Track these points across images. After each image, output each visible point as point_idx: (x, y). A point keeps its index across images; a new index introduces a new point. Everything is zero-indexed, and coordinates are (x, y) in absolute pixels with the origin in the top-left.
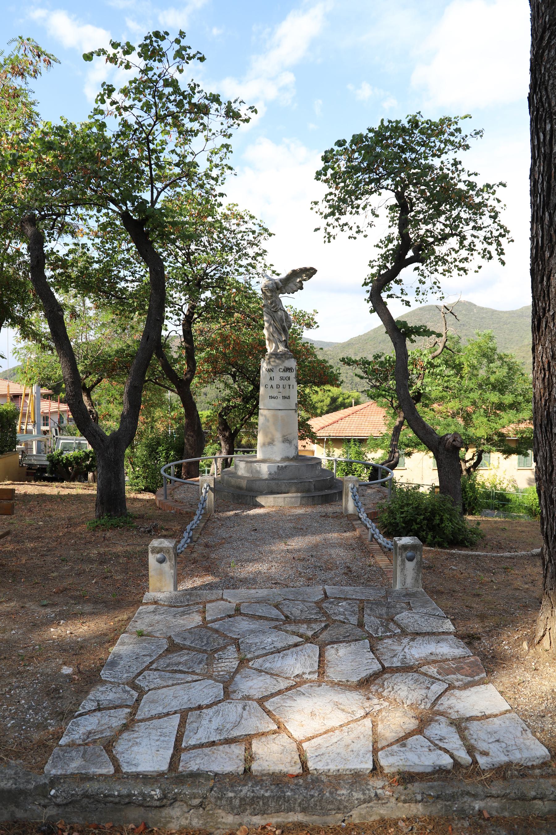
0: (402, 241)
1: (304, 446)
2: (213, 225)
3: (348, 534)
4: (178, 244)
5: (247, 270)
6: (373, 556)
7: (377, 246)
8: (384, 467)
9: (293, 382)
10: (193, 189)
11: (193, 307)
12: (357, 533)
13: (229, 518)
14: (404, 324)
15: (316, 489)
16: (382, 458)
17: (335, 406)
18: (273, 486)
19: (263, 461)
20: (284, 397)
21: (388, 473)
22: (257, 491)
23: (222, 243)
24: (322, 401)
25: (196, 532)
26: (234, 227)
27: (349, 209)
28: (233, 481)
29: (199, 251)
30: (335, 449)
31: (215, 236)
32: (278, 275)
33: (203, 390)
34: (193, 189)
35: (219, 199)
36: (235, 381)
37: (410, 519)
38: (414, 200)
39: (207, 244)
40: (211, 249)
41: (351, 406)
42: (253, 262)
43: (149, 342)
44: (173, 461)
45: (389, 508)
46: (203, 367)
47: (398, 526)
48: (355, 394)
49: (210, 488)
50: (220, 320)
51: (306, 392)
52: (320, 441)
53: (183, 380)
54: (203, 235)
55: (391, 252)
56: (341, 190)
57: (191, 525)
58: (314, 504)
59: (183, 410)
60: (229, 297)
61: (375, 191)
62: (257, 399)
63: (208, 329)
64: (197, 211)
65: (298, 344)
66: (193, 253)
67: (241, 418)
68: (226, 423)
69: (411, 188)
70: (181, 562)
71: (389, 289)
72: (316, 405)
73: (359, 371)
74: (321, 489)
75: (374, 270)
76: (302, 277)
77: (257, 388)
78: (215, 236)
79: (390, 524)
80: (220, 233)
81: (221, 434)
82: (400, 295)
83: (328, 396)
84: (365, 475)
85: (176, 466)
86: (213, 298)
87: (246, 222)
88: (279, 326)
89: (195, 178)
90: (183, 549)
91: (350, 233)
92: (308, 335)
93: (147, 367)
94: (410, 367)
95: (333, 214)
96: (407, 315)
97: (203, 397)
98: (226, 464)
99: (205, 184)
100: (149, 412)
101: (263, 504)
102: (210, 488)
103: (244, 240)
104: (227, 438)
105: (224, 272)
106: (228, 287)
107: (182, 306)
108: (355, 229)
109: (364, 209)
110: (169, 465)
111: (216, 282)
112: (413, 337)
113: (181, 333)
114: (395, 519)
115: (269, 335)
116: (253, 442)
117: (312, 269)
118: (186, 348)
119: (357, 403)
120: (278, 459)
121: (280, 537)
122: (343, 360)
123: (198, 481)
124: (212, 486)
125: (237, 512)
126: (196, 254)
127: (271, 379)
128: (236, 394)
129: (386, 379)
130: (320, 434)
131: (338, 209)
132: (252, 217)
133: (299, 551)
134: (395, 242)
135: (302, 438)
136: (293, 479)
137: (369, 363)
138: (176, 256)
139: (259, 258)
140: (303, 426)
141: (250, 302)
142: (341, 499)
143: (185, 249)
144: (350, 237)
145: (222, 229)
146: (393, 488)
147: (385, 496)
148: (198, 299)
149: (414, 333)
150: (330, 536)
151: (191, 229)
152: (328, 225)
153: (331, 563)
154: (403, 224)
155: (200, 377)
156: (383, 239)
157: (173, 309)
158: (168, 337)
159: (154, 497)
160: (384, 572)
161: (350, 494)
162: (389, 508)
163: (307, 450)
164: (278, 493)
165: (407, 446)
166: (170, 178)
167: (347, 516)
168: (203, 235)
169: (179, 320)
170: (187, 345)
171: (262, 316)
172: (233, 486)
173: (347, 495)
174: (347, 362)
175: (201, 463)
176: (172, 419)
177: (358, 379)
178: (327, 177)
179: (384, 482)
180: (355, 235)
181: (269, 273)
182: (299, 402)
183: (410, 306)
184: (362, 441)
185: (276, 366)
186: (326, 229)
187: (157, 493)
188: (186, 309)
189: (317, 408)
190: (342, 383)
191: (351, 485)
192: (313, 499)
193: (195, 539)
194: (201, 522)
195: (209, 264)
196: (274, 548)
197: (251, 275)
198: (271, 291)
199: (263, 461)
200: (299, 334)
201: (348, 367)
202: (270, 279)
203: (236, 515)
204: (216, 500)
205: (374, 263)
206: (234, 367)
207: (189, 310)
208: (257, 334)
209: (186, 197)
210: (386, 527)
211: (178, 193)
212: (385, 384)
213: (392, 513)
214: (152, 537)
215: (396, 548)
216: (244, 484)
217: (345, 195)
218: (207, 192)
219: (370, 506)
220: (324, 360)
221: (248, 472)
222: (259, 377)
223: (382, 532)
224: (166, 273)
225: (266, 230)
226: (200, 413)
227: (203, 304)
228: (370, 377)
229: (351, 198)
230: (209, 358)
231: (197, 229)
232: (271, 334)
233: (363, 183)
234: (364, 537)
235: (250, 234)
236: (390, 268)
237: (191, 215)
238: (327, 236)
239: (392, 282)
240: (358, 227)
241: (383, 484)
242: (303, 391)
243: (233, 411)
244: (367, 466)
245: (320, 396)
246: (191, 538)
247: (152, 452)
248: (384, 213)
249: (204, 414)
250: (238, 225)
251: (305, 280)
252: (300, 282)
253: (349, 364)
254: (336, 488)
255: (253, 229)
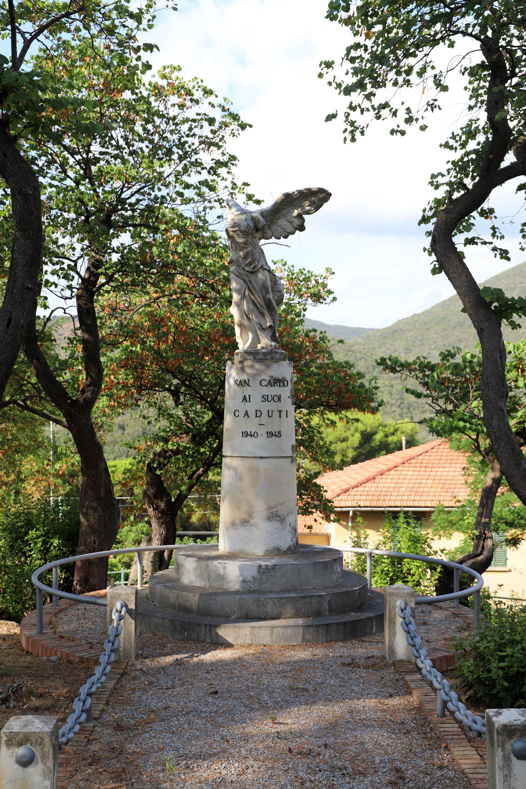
0: (493, 133)
1: (310, 527)
2: (134, 108)
3: (396, 702)
4: (67, 141)
5: (199, 195)
6: (446, 748)
7: (447, 145)
8: (464, 566)
9: (287, 404)
10: (92, 37)
11: (96, 264)
12: (414, 699)
13: (164, 669)
14: (498, 294)
15: (334, 610)
16: (461, 550)
17: (369, 448)
18: (249, 610)
19: (231, 556)
20: (270, 434)
21: (472, 578)
22: (219, 616)
23: (151, 141)
24: (345, 440)
25: (98, 699)
26: (173, 112)
27: (392, 75)
28: (172, 596)
29: (107, 157)
30: (369, 532)
31: (138, 128)
32: (258, 202)
33: (117, 420)
34: (92, 37)
35: (145, 56)
36: (177, 403)
37: (518, 672)
38: (519, 53)
39: (122, 142)
40: (131, 154)
41: (400, 449)
42: (210, 178)
43: (11, 330)
44: (57, 557)
45: (476, 648)
46: (115, 376)
47: (495, 686)
48: (407, 426)
49: (129, 611)
50: (150, 289)
51: (313, 423)
52: (342, 516)
53: (77, 401)
54: (115, 125)
55: (473, 156)
56: (377, 38)
57: (88, 685)
58: (329, 641)
59: (78, 458)
60: (165, 244)
61: (443, 39)
62: (220, 437)
63: (123, 305)
64: (102, 80)
65: (297, 332)
66: (97, 160)
67: (190, 472)
68: (162, 483)
69: (513, 30)
70: (67, 762)
71: (469, 227)
72: (332, 448)
73: (413, 383)
74: (344, 610)
75: (441, 193)
76: (302, 207)
77: (219, 416)
78: (138, 128)
79: (479, 681)
80: (147, 121)
81: (151, 503)
82: (489, 239)
83: (356, 430)
84: (428, 584)
85: (63, 567)
86: (135, 246)
87: (197, 102)
88: (259, 300)
89: (98, 14)
90: (71, 735)
91: (392, 123)
92: (315, 314)
93: (7, 378)
94: (511, 375)
95: (360, 85)
96: (506, 275)
97: (117, 434)
98: (161, 562)
99: (116, 27)
100: (13, 463)
101: (230, 640)
102: (129, 611)
103: (194, 135)
104: (163, 512)
105: (156, 197)
106: (163, 227)
107: (75, 262)
108: (402, 115)
109: (420, 74)
110: (49, 565)
111: (141, 216)
112: (515, 317)
113: (74, 312)
114: (489, 671)
115: (242, 317)
116: (213, 519)
117: (321, 191)
118: (84, 342)
119: (411, 443)
120: (260, 551)
121: (264, 708)
122: (382, 362)
123: (105, 596)
124: (132, 606)
125: (179, 657)
126: (102, 163)
127: (245, 399)
128: (181, 428)
129: (465, 398)
130: (341, 503)
131: (371, 77)
132: (208, 92)
133: (301, 735)
134: (481, 138)
135: (306, 511)
136: (289, 591)
137: (432, 368)
138: (63, 165)
139: (222, 171)
140: (308, 487)
141: (204, 255)
142: (382, 630)
143: (79, 153)
144: (393, 132)
145: (152, 114)
146: (484, 609)
147: (468, 626)
148: (105, 249)
149: (516, 310)
150: (360, 704)
151: (92, 115)
152: (352, 108)
153: (363, 761)
154: (495, 104)
155: (110, 397)
156: (458, 132)
157: (57, 267)
158: (49, 319)
159: (17, 630)
160: (469, 781)
161: (399, 621)
162: (476, 648)
163: (316, 534)
164: (260, 619)
165: (511, 525)
166: (48, 13)
167: (394, 664)
168: (115, 125)
169: (70, 287)
170: (86, 336)
171: (227, 281)
172: (172, 606)
173: (393, 622)
174: (390, 365)
175: (112, 560)
176: (57, 475)
177: (412, 398)
178: (351, 13)
179: (466, 597)
180: (403, 126)
181: (240, 199)
182: (300, 443)
183: (508, 259)
184: (421, 517)
185: (254, 376)
186: (347, 115)
187: (24, 621)
188: (83, 266)
189: (333, 454)
190: (380, 405)
191: (399, 603)
192: (327, 631)
193: (96, 714)
194: (109, 679)
195: (128, 182)
196: (250, 729)
197: (206, 204)
198: (245, 233)
199: (231, 556)
200: (298, 315)
201: (391, 374)
202: (243, 212)
203: (178, 663)
204: (139, 635)
205: (440, 180)
206: (175, 377)
207: (88, 269)
208: (220, 315)
209: (81, 51)
210: (471, 687)
211: (64, 42)
212: (463, 406)
213: (483, 659)
214: (10, 712)
215: (491, 732)
216: (193, 600)
217: (383, 49)
218: (120, 44)
219: (439, 644)
220: (347, 363)
221: (200, 576)
222: (223, 395)
223: (464, 698)
224: (43, 197)
225: (235, 117)
226: (109, 463)
227: (115, 257)
228: (435, 394)
229: (396, 54)
230: (127, 359)
231: (102, 115)
232: (245, 315)
233: (419, 24)
234: (428, 706)
235: (206, 124)
236: (470, 187)
237: (91, 87)
238: (350, 129)
239: (475, 214)
240: (408, 110)
241: (464, 601)
242: (308, 421)
243: (173, 460)
244: (432, 565)
245: (340, 429)
246: (88, 711)
247: (16, 540)
248: (458, 82)
249: (119, 465)
250: (182, 106)
251: (308, 213)
252: (300, 216)
253: (393, 370)
254: (370, 607)
255: (211, 116)
